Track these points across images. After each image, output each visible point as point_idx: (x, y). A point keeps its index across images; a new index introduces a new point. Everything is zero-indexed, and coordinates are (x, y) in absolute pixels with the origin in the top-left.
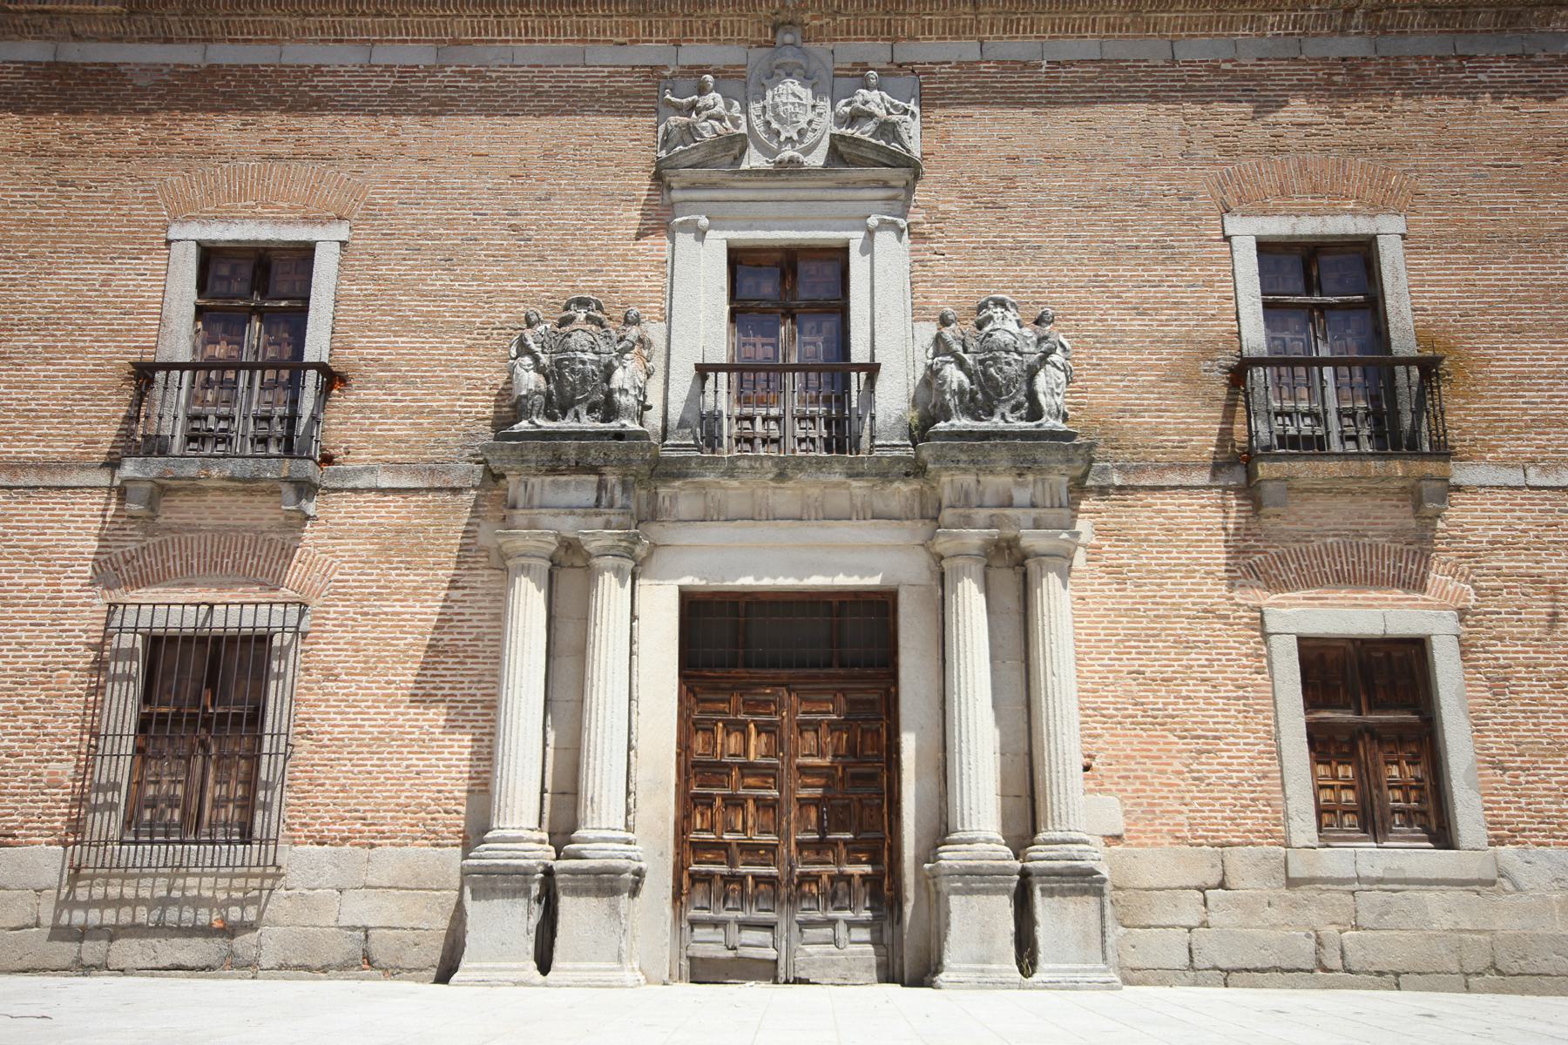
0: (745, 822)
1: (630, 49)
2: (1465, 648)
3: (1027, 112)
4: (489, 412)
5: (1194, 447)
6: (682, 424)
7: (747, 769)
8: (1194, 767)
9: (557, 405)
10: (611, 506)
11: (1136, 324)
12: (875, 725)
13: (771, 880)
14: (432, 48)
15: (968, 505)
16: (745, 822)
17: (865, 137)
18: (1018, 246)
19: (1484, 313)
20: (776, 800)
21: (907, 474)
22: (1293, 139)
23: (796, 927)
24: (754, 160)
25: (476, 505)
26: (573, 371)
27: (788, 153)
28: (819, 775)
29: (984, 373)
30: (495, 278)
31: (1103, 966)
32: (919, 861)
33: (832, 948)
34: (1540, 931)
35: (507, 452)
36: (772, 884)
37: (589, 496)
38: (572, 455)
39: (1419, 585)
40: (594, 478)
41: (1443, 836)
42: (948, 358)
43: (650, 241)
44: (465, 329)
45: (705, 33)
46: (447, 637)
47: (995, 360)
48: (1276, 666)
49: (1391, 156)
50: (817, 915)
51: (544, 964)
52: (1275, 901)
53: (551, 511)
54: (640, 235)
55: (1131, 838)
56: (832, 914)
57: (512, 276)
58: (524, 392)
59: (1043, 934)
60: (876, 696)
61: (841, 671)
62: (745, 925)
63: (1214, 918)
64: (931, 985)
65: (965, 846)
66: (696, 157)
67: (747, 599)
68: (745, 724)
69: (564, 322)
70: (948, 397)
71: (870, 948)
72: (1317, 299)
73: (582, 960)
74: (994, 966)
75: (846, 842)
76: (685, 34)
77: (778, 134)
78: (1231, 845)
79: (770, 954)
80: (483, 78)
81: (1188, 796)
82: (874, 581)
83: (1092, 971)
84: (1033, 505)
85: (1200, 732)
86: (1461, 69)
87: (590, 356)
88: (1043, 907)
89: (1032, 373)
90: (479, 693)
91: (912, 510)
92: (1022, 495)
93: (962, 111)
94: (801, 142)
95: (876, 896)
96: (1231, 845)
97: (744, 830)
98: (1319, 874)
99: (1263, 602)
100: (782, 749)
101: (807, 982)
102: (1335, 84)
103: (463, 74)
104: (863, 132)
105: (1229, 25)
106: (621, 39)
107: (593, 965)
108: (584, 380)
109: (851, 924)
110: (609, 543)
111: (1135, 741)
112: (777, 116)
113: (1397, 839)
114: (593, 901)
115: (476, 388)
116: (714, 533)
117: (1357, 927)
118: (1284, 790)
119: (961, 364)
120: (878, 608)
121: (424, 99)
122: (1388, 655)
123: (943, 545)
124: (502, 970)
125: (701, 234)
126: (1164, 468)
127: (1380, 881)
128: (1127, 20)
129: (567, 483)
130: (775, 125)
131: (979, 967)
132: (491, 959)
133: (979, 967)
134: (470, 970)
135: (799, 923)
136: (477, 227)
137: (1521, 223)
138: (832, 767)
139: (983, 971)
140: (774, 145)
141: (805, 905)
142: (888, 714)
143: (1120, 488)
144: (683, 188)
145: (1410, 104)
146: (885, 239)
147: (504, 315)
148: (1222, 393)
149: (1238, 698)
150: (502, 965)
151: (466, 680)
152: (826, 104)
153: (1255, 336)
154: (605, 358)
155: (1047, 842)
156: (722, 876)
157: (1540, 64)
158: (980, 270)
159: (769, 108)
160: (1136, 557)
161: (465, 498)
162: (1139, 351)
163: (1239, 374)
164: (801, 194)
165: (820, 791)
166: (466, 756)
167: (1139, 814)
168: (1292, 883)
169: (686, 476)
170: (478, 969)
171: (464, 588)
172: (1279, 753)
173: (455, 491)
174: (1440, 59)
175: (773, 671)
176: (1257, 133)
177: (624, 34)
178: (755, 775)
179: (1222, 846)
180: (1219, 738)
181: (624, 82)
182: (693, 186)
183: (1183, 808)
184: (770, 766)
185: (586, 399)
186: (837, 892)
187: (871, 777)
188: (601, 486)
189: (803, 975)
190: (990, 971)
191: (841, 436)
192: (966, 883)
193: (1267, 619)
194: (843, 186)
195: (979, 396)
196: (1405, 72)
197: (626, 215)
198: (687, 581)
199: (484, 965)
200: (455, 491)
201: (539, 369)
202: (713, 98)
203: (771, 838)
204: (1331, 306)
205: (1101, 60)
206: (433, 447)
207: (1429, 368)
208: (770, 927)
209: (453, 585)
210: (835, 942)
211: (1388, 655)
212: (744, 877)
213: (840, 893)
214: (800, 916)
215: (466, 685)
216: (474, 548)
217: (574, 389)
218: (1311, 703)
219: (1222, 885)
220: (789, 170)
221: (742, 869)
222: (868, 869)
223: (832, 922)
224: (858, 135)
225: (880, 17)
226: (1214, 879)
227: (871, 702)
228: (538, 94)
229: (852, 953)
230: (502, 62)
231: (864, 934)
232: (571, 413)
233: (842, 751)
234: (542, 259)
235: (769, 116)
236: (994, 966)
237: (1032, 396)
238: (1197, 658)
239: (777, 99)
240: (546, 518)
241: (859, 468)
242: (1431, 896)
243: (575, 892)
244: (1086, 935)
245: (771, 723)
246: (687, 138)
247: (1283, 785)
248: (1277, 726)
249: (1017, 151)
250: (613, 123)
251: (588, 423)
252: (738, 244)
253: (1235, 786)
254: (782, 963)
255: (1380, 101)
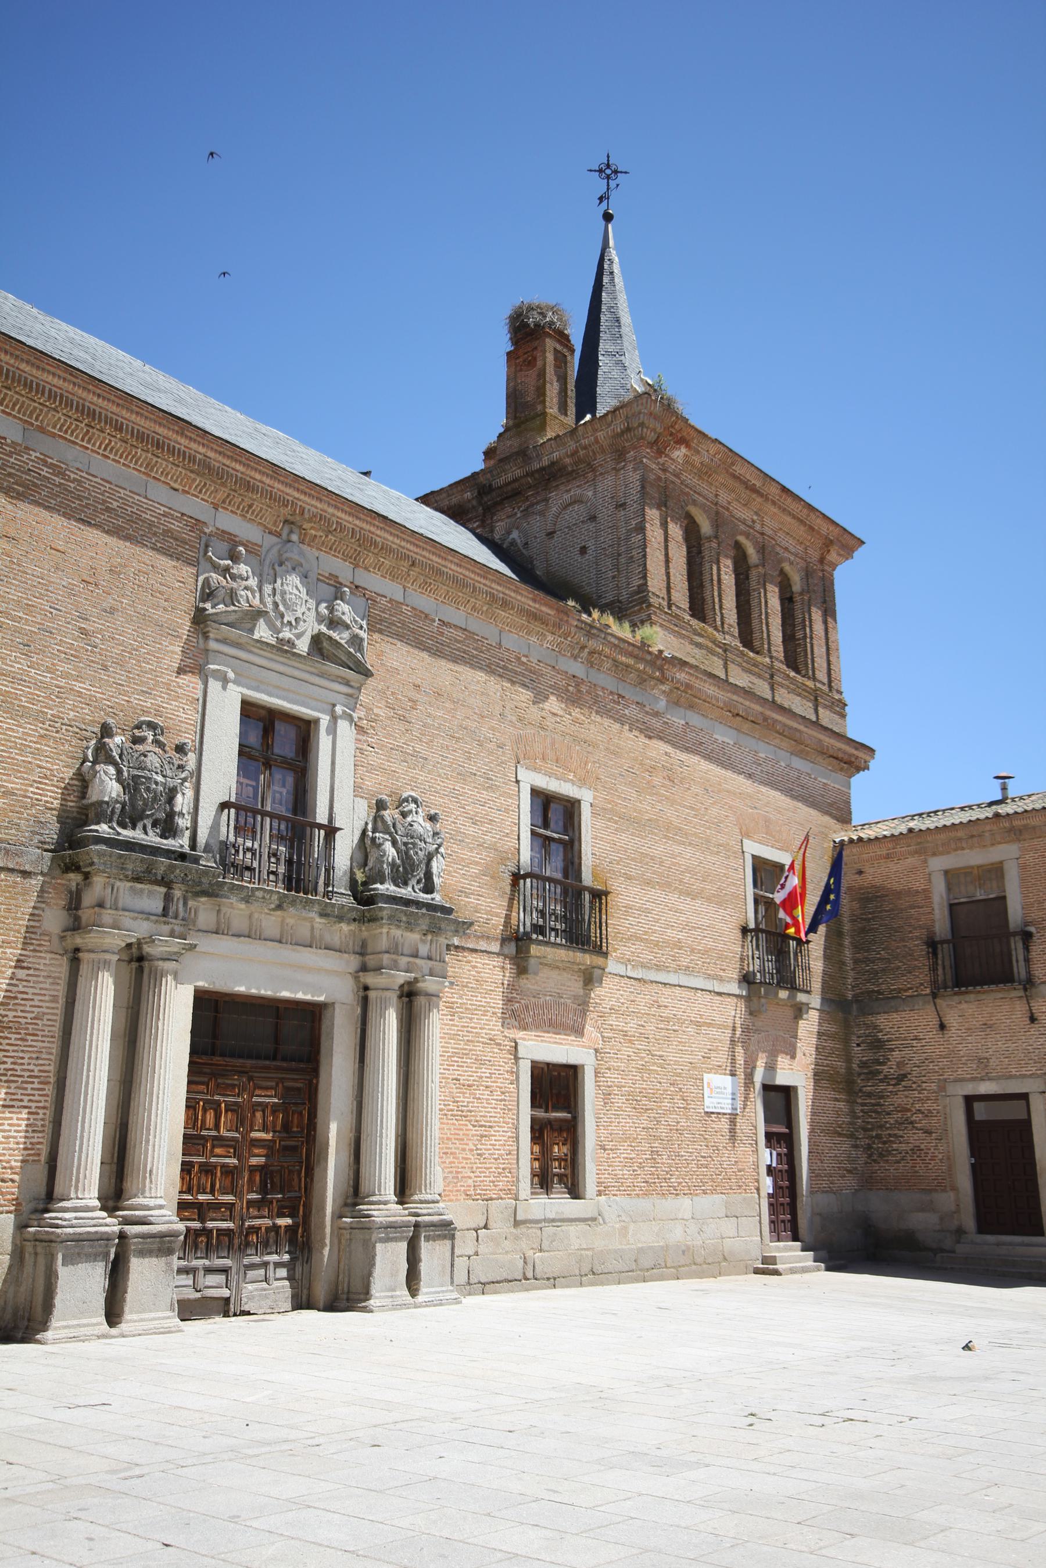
0: (213, 1186)
1: (182, 497)
2: (597, 1073)
3: (425, 655)
4: (56, 803)
5: (493, 925)
6: (207, 849)
7: (219, 1140)
8: (479, 1146)
9: (131, 817)
10: (176, 918)
11: (471, 830)
12: (300, 1108)
13: (228, 1232)
14: (19, 426)
15: (396, 953)
16: (213, 1186)
17: (343, 642)
18: (415, 754)
19: (618, 864)
20: (235, 1167)
21: (354, 920)
22: (550, 721)
23: (242, 1269)
24: (262, 632)
25: (42, 891)
26: (148, 789)
27: (286, 634)
28: (263, 1147)
29: (407, 853)
30: (65, 675)
31: (451, 1288)
32: (338, 1216)
33: (264, 1285)
34: (610, 1247)
35: (113, 859)
36: (228, 1235)
37: (156, 905)
38: (161, 871)
39: (579, 1032)
40: (163, 890)
41: (575, 1192)
42: (387, 837)
43: (186, 679)
44: (39, 717)
45: (238, 508)
46: (11, 1014)
47: (414, 844)
48: (521, 1080)
49: (590, 749)
50: (256, 1260)
51: (113, 1314)
52: (509, 1236)
53: (132, 914)
54: (180, 671)
55: (446, 1196)
56: (267, 1258)
57: (79, 678)
58: (106, 799)
59: (424, 1267)
60: (301, 1085)
61: (285, 1064)
62: (209, 1271)
63: (482, 1249)
64: (365, 1310)
65: (382, 1207)
66: (232, 618)
67: (227, 999)
68: (219, 1103)
69: (137, 740)
70: (385, 866)
71: (287, 1283)
72: (549, 833)
73: (144, 1311)
74: (398, 1293)
75: (278, 1200)
76: (224, 502)
77: (282, 616)
78: (491, 1199)
79: (225, 1293)
80: (62, 474)
81: (475, 1166)
82: (322, 999)
83: (446, 1291)
84: (430, 958)
85: (483, 1123)
86: (619, 703)
87: (160, 778)
88: (426, 1249)
89: (430, 858)
90: (36, 1069)
91: (347, 946)
92: (424, 950)
93: (390, 640)
94: (296, 628)
95: (293, 1242)
96: (491, 1199)
97: (212, 1192)
98: (530, 1217)
99: (517, 1036)
100: (242, 1125)
101: (248, 1313)
102: (568, 691)
103: (45, 463)
104: (341, 637)
105: (529, 633)
106: (176, 486)
107: (153, 1315)
108: (155, 799)
109: (277, 1265)
110: (176, 950)
111: (452, 1127)
112: (284, 600)
113: (557, 1193)
114: (154, 1261)
115: (46, 777)
116: (224, 944)
117: (541, 1251)
118: (518, 1163)
119: (394, 843)
120: (310, 1017)
121: (10, 475)
122: (559, 1074)
123: (370, 979)
124: (85, 1326)
125: (225, 681)
126: (479, 937)
127: (553, 1220)
128: (485, 609)
129: (142, 890)
130: (281, 608)
131: (390, 1294)
132: (75, 1317)
133: (390, 1294)
134: (59, 1328)
135: (245, 1266)
136: (53, 619)
137: (635, 811)
138: (273, 1141)
139: (392, 1297)
140: (278, 624)
141: (249, 1252)
142: (310, 1100)
143: (457, 947)
144: (217, 640)
145: (598, 719)
146: (343, 725)
147: (72, 713)
148: (508, 889)
149: (501, 1100)
150: (85, 1321)
151: (27, 1056)
152: (312, 604)
153: (526, 855)
154: (171, 783)
155: (421, 1202)
156: (196, 1230)
157: (647, 713)
158: (394, 766)
159: (278, 592)
160: (461, 998)
161: (34, 882)
162: (471, 850)
163: (517, 878)
164: (296, 673)
165: (263, 1159)
166: (23, 1128)
167: (450, 1179)
168: (517, 1223)
169: (217, 896)
170: (65, 1327)
171: (29, 968)
172: (517, 1138)
173: (26, 874)
174: (612, 693)
175: (241, 1061)
176: (534, 713)
177: (181, 484)
178: (222, 1146)
179: (487, 1200)
180: (490, 1127)
181: (175, 526)
182: (224, 641)
183: (472, 1175)
184: (233, 1139)
185: (153, 814)
186: (270, 1240)
187: (294, 1149)
188: (168, 898)
189: (246, 1308)
190: (397, 1296)
191: (298, 880)
192: (387, 1234)
193: (519, 1048)
194: (321, 675)
195: (401, 869)
196: (597, 696)
197: (171, 648)
198: (200, 984)
199: (71, 1323)
200: (26, 874)
201: (119, 780)
202: (243, 569)
203: (229, 1198)
204: (553, 839)
205: (465, 630)
206: (7, 828)
207: (599, 895)
208: (225, 1271)
209: (19, 964)
210: (266, 1280)
211: (559, 1074)
212: (211, 1231)
213: (271, 1241)
214: (246, 1261)
215: (25, 1061)
216: (39, 931)
217: (146, 804)
218: (534, 1104)
219: (486, 1227)
220: (284, 648)
221: (210, 1225)
222: (288, 1221)
223: (265, 1264)
224: (337, 638)
225: (355, 547)
226: (482, 1225)
227: (299, 1089)
228: (108, 509)
229: (277, 1288)
230: (80, 466)
231: (283, 1272)
232: (140, 825)
233: (278, 1128)
234: (105, 668)
235: (278, 598)
236: (398, 1293)
237: (429, 875)
238: (485, 1072)
239: (285, 587)
240: (127, 920)
241: (329, 910)
242: (572, 1229)
243: (142, 1253)
244: (444, 1266)
245: (236, 1103)
246: (228, 600)
247: (518, 1159)
248: (518, 1120)
249: (418, 682)
250: (165, 563)
251: (153, 838)
252: (249, 699)
253: (496, 1159)
254: (232, 1300)
255: (586, 711)
